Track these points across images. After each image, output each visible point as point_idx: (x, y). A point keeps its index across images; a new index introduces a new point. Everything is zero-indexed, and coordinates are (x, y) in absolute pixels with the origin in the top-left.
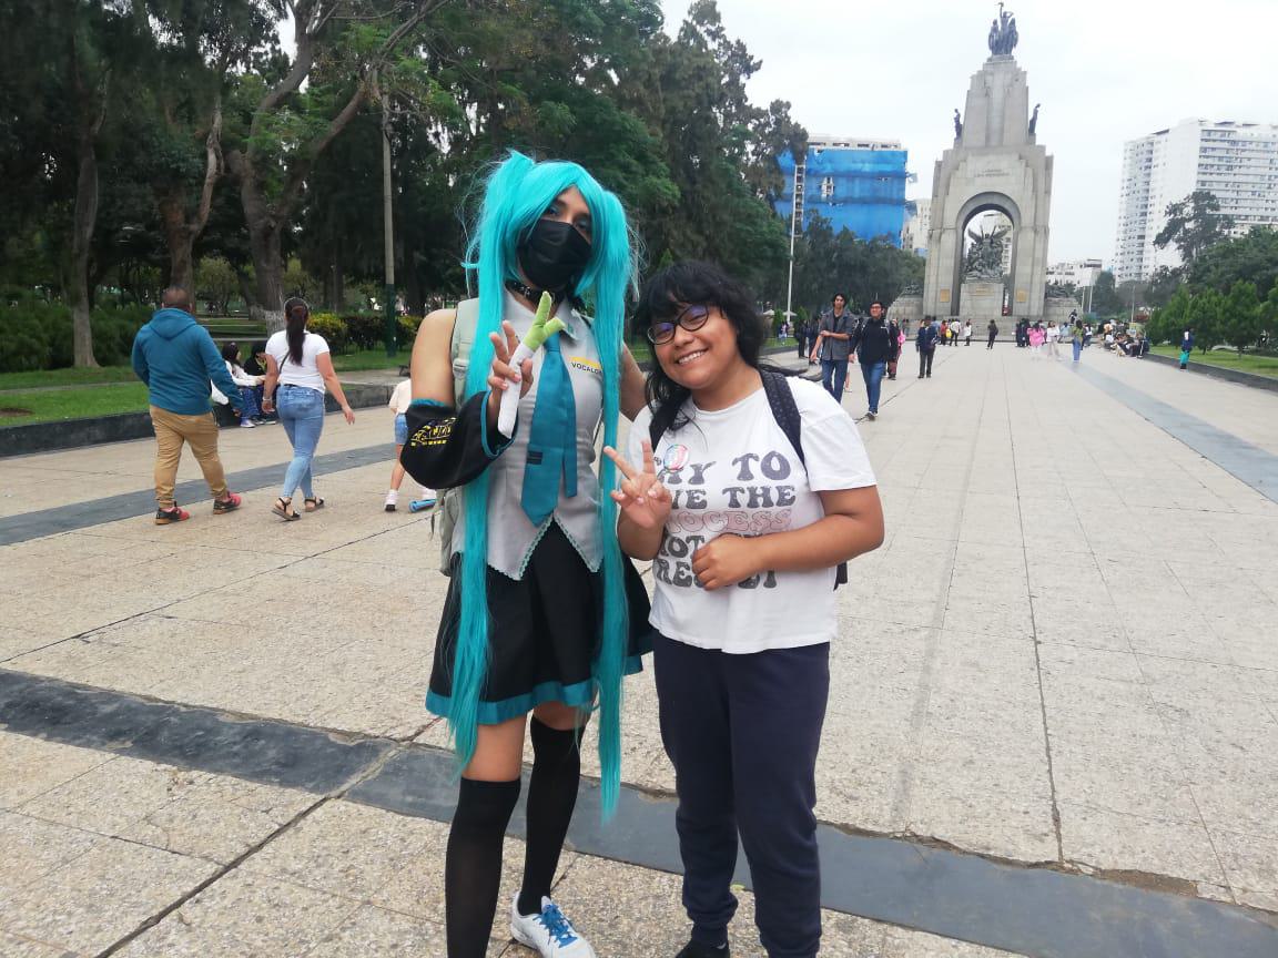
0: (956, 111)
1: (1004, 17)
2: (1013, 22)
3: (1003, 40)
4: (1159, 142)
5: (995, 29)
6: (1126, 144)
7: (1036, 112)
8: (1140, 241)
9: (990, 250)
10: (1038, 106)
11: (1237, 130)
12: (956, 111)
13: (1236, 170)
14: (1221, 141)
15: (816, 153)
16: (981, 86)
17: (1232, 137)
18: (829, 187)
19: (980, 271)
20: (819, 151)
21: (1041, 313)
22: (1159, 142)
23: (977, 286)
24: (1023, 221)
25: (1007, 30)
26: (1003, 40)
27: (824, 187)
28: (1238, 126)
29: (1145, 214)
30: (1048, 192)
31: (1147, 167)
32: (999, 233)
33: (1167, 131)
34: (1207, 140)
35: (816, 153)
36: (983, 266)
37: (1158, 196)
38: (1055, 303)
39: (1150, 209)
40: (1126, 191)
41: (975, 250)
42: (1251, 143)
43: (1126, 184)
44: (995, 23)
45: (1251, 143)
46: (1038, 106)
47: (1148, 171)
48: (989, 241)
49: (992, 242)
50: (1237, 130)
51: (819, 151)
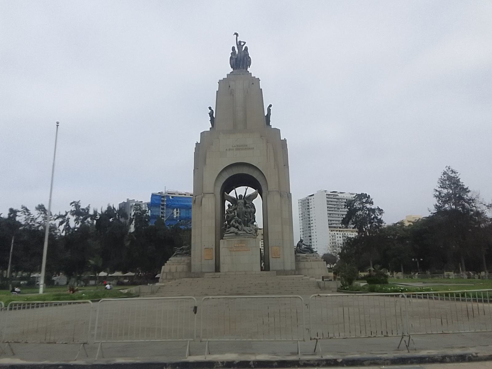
0: (210, 108)
1: (239, 44)
2: (246, 49)
3: (240, 60)
4: (311, 199)
5: (234, 53)
6: (299, 200)
7: (269, 110)
8: (310, 238)
9: (244, 209)
10: (270, 106)
11: (339, 194)
12: (210, 108)
13: (341, 210)
14: (333, 198)
15: (171, 198)
16: (226, 88)
17: (337, 197)
18: (177, 213)
19: (237, 228)
20: (172, 197)
21: (294, 268)
22: (311, 199)
23: (235, 241)
24: (269, 188)
25: (243, 54)
26: (240, 60)
27: (175, 213)
28: (338, 193)
29: (310, 227)
30: (286, 165)
31: (308, 209)
32: (250, 196)
33: (313, 195)
34: (328, 198)
35: (171, 198)
36: (240, 223)
37: (314, 220)
38: (303, 258)
39: (311, 225)
40: (301, 218)
41: (231, 210)
42: (344, 199)
43: (301, 215)
44: (233, 48)
45: (344, 199)
46: (270, 106)
47: (308, 210)
48: (243, 201)
49: (245, 203)
50: (339, 194)
51: (172, 197)
